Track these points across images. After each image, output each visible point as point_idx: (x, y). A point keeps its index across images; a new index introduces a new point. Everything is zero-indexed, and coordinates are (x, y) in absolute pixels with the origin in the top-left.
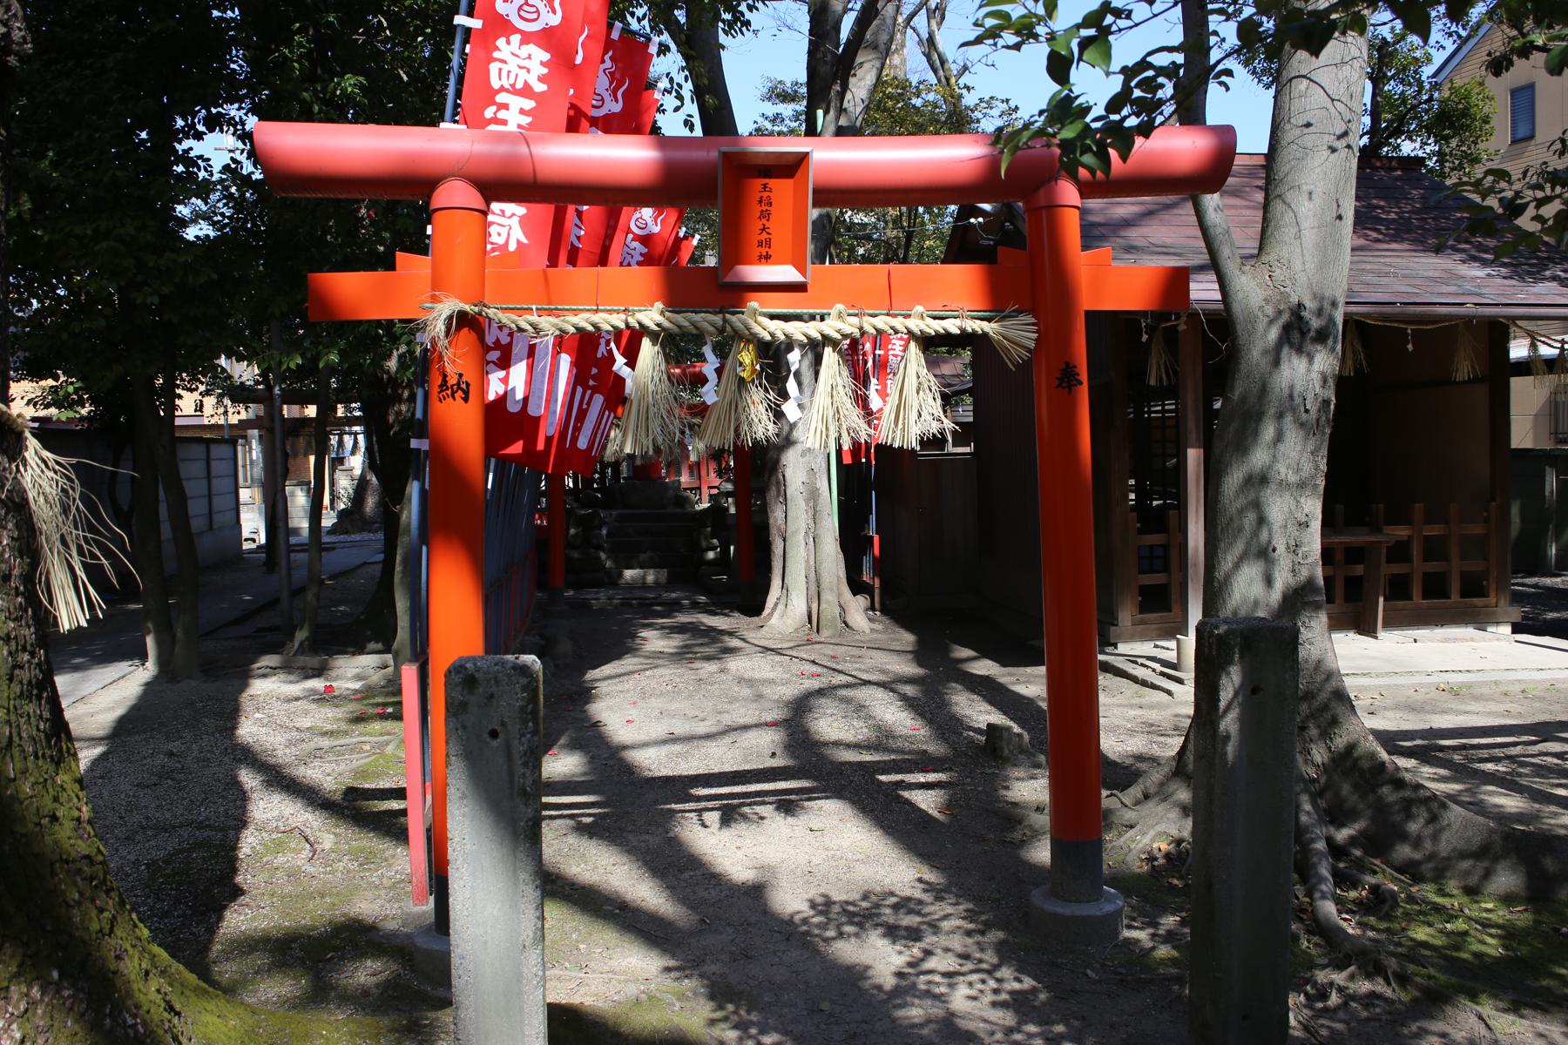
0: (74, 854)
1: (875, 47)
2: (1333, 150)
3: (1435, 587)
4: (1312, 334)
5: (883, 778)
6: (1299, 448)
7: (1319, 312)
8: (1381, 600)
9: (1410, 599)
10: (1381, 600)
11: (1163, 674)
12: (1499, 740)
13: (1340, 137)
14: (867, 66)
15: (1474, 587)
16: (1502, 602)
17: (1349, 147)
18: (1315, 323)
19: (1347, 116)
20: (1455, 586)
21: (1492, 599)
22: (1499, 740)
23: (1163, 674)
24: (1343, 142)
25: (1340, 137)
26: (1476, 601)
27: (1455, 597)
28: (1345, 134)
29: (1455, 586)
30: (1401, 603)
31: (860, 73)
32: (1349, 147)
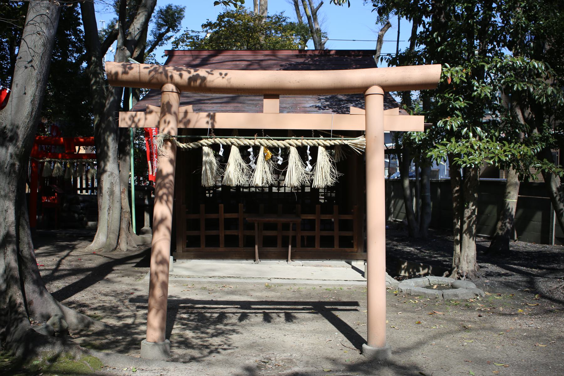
0: (48, 305)
1: (145, 6)
2: (26, 67)
3: (327, 242)
4: (8, 138)
5: (327, 307)
6: (4, 182)
7: (12, 130)
8: (290, 247)
9: (314, 247)
10: (290, 247)
11: (213, 270)
12: (222, 306)
13: (29, 62)
14: (141, 14)
15: (250, 242)
16: (359, 250)
17: (32, 66)
18: (9, 134)
19: (33, 54)
20: (336, 242)
21: (355, 249)
22: (222, 306)
23: (213, 270)
24: (30, 65)
25: (29, 62)
26: (347, 249)
27: (336, 248)
28: (31, 61)
29: (336, 242)
30: (309, 249)
31: (138, 17)
32: (32, 66)
